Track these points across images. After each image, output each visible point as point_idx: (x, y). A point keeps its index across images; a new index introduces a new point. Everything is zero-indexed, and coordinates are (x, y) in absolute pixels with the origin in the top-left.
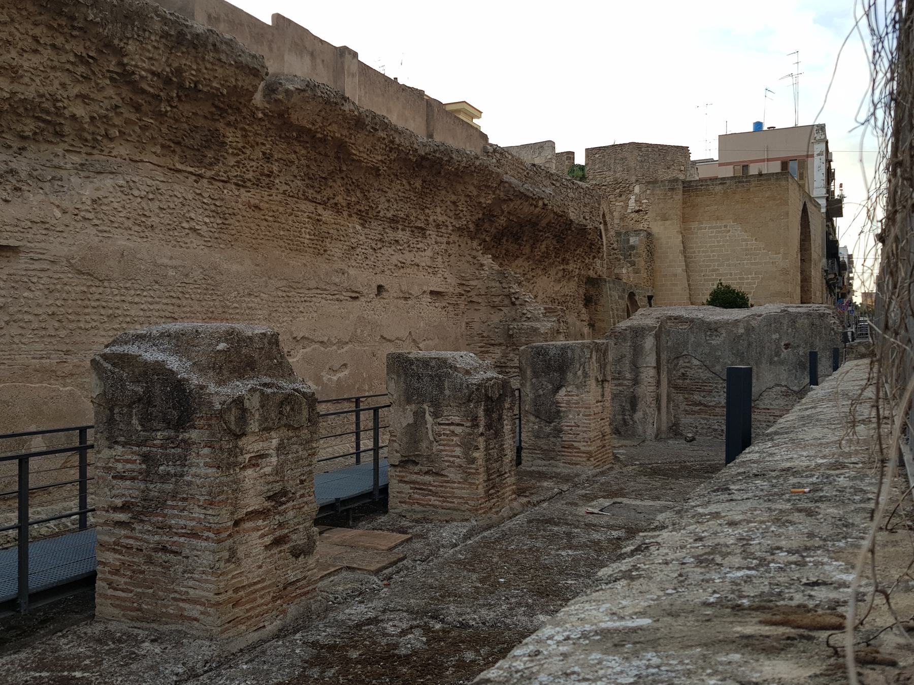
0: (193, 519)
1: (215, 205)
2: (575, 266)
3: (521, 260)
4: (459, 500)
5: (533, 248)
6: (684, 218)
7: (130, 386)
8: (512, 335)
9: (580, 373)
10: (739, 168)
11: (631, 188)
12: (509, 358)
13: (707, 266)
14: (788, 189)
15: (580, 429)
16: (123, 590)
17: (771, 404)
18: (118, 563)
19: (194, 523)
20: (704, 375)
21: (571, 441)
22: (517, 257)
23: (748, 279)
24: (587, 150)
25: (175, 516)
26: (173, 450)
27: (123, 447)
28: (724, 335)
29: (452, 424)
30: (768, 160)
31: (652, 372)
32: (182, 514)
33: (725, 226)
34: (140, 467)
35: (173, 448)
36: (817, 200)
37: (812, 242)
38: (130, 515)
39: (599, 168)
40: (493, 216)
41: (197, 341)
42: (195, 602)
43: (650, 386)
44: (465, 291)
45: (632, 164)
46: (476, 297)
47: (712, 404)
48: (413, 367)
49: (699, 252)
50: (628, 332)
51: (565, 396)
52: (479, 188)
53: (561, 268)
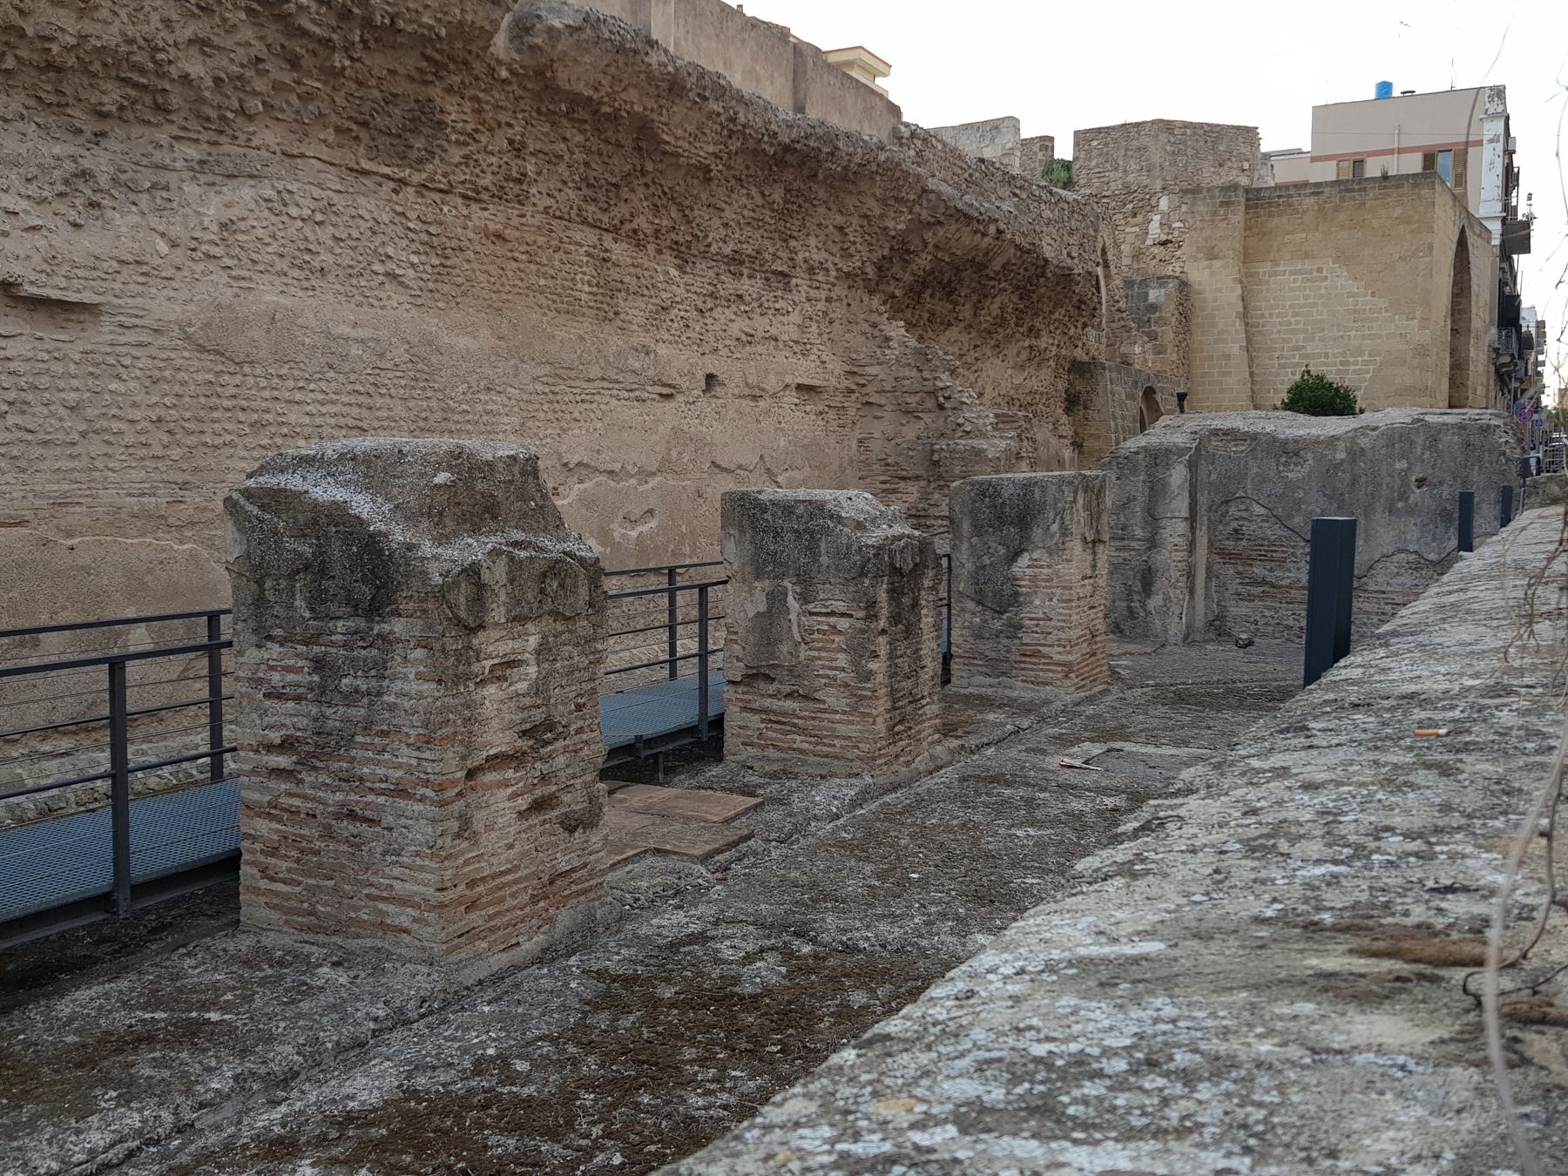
0: (399, 766)
1: (429, 233)
6: (1245, 254)
7: (290, 544)
9: (1055, 528)
10: (1347, 165)
13: (1284, 340)
16: (284, 881)
19: (400, 773)
22: (950, 324)
23: (1355, 363)
24: (1076, 133)
25: (369, 761)
26: (363, 652)
29: (832, 614)
31: (1182, 527)
34: (309, 678)
37: (1473, 299)
38: (294, 758)
40: (908, 252)
45: (1156, 159)
52: (883, 202)
53: (1027, 343)
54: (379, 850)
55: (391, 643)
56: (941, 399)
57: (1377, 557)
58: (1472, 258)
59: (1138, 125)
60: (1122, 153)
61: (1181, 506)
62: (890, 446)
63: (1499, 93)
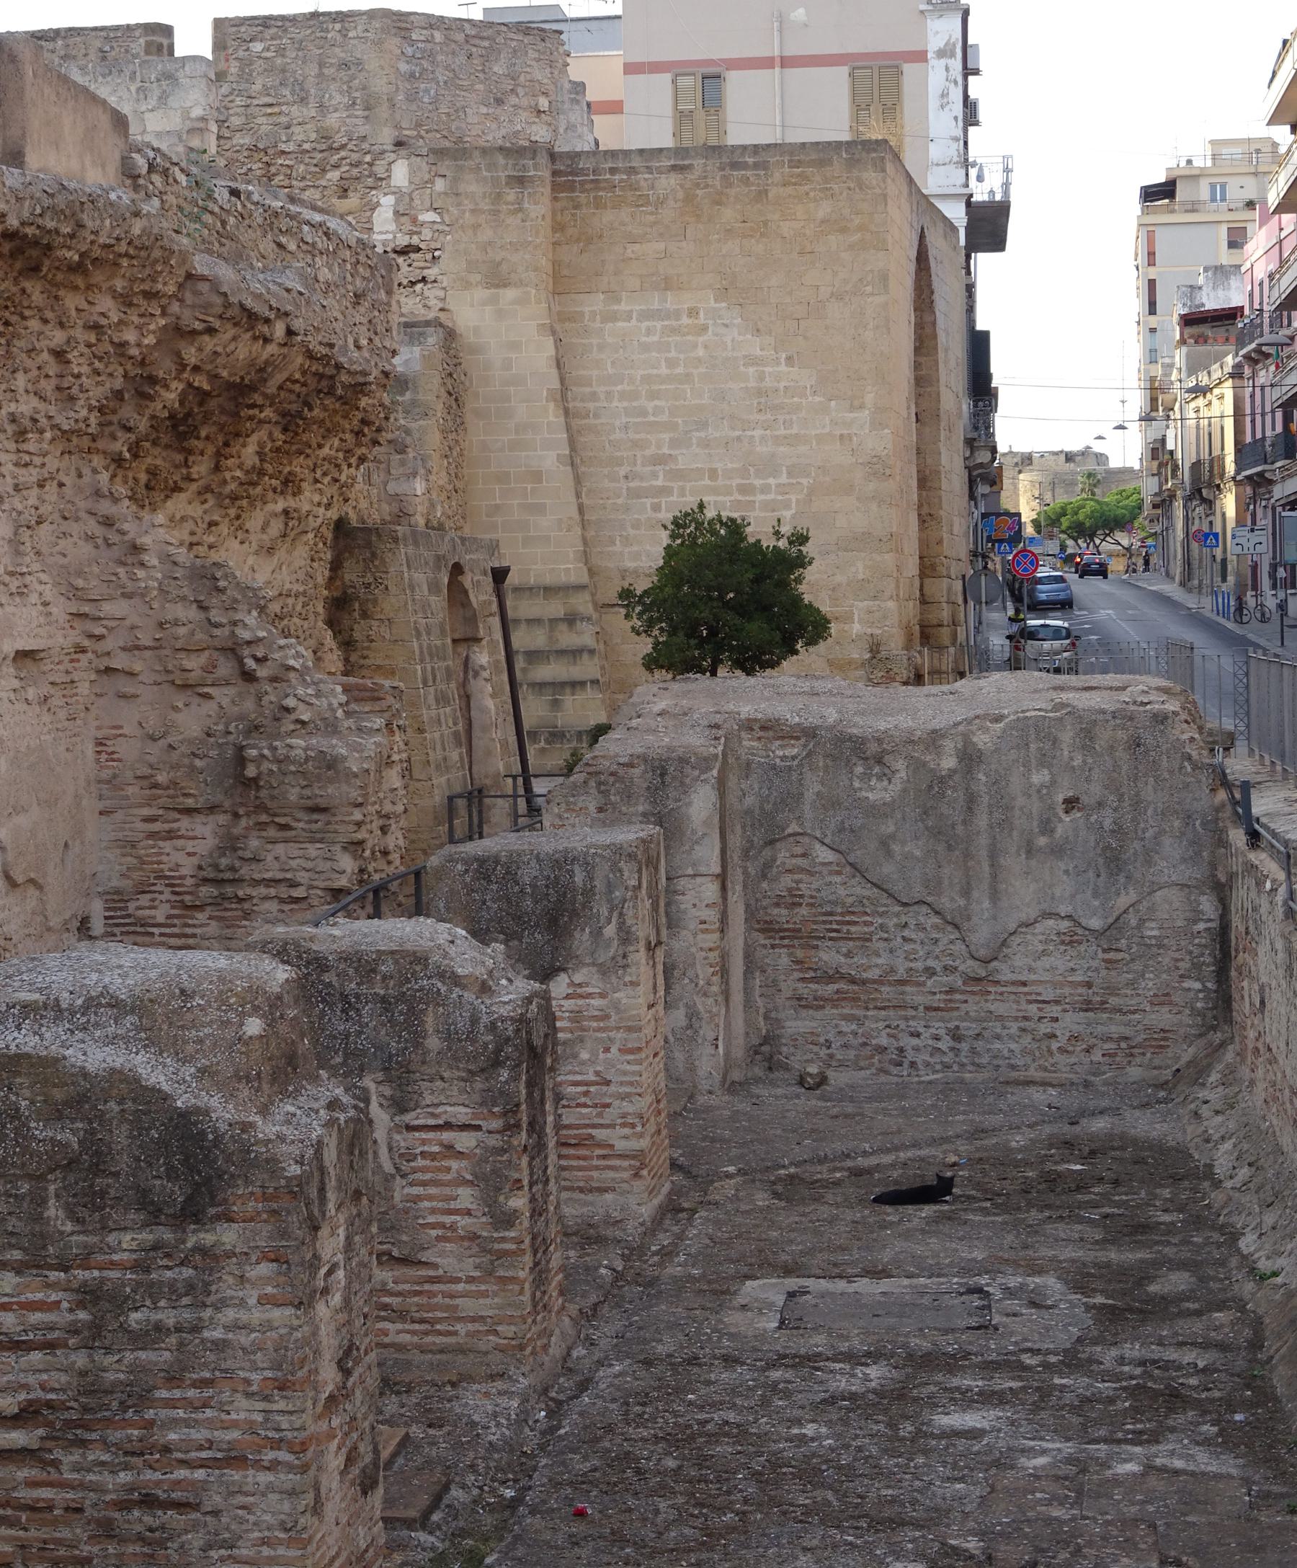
0: (235, 1425)
2: (316, 498)
3: (183, 496)
4: (470, 1327)
6: (557, 276)
7: (39, 1130)
8: (255, 780)
9: (610, 931)
11: (380, 169)
12: (248, 855)
13: (636, 444)
14: (885, 196)
15: (613, 1088)
17: (1030, 970)
20: (847, 890)
21: (587, 1126)
22: (177, 489)
23: (765, 489)
24: (219, 24)
25: (175, 1423)
26: (169, 1274)
27: (18, 1272)
28: (903, 774)
29: (448, 1126)
30: (786, 62)
31: (710, 890)
32: (201, 1416)
33: (693, 312)
34: (70, 1317)
35: (168, 1268)
36: (941, 205)
37: (941, 355)
38: (41, 1432)
39: (266, 91)
40: (152, 380)
41: (189, 1016)
43: (706, 931)
44: (91, 636)
45: (380, 85)
46: (123, 655)
47: (873, 974)
48: (326, 978)
49: (609, 394)
50: (637, 772)
51: (568, 997)
52: (126, 301)
53: (280, 505)
54: (198, 1543)
55: (216, 1258)
56: (250, 663)
57: (1012, 926)
58: (936, 284)
59: (342, 17)
60: (313, 70)
61: (708, 855)
62: (155, 750)
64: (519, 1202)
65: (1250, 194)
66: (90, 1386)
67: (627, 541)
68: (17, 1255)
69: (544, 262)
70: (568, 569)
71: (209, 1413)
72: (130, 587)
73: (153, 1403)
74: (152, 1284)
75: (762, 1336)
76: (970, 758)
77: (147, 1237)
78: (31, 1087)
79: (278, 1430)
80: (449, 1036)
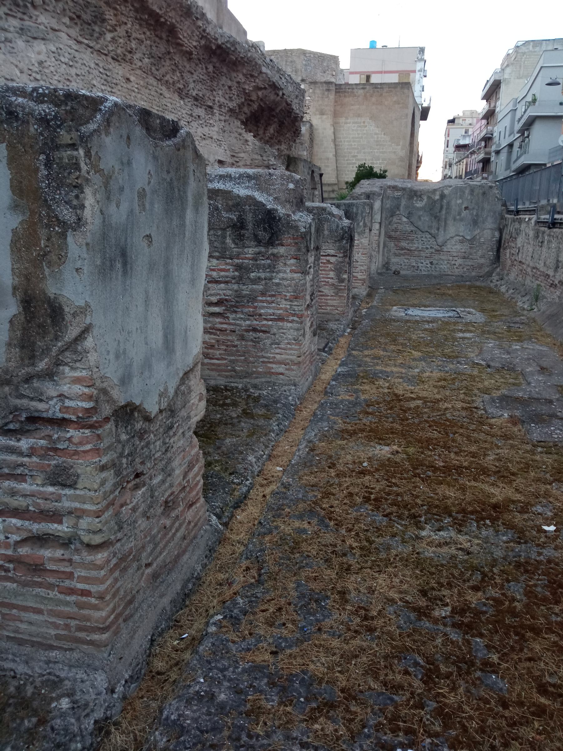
0: (281, 309)
1: (107, 75)
5: (265, 130)
7: (224, 214)
9: (361, 224)
13: (350, 153)
16: (217, 359)
18: (214, 341)
19: (281, 312)
23: (377, 164)
25: (264, 307)
26: (263, 262)
27: (218, 260)
29: (328, 255)
34: (233, 274)
42: (280, 363)
45: (299, 67)
55: (278, 257)
59: (292, 51)
60: (284, 63)
61: (378, 217)
63: (422, 50)
64: (345, 276)
65: (470, 122)
66: (239, 295)
67: (346, 174)
68: (217, 254)
69: (332, 110)
70: (333, 180)
71: (273, 305)
72: (245, 150)
73: (257, 301)
74: (257, 265)
75: (402, 316)
76: (443, 196)
77: (257, 250)
78: (222, 199)
79: (294, 311)
80: (330, 231)
